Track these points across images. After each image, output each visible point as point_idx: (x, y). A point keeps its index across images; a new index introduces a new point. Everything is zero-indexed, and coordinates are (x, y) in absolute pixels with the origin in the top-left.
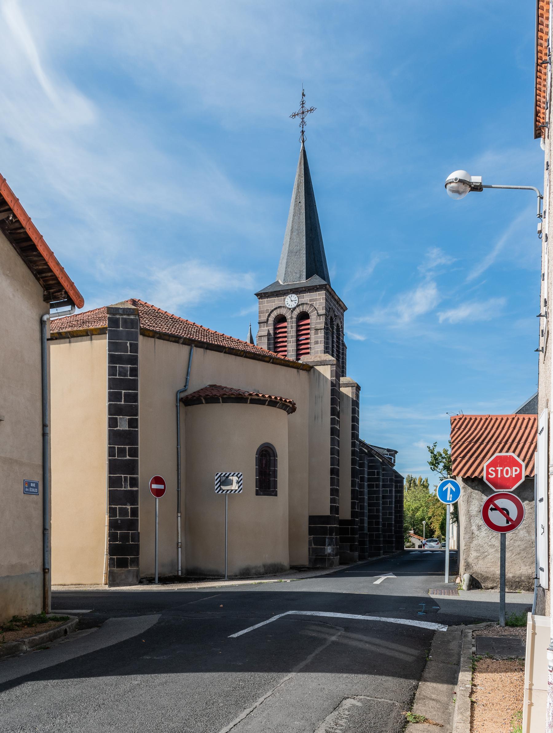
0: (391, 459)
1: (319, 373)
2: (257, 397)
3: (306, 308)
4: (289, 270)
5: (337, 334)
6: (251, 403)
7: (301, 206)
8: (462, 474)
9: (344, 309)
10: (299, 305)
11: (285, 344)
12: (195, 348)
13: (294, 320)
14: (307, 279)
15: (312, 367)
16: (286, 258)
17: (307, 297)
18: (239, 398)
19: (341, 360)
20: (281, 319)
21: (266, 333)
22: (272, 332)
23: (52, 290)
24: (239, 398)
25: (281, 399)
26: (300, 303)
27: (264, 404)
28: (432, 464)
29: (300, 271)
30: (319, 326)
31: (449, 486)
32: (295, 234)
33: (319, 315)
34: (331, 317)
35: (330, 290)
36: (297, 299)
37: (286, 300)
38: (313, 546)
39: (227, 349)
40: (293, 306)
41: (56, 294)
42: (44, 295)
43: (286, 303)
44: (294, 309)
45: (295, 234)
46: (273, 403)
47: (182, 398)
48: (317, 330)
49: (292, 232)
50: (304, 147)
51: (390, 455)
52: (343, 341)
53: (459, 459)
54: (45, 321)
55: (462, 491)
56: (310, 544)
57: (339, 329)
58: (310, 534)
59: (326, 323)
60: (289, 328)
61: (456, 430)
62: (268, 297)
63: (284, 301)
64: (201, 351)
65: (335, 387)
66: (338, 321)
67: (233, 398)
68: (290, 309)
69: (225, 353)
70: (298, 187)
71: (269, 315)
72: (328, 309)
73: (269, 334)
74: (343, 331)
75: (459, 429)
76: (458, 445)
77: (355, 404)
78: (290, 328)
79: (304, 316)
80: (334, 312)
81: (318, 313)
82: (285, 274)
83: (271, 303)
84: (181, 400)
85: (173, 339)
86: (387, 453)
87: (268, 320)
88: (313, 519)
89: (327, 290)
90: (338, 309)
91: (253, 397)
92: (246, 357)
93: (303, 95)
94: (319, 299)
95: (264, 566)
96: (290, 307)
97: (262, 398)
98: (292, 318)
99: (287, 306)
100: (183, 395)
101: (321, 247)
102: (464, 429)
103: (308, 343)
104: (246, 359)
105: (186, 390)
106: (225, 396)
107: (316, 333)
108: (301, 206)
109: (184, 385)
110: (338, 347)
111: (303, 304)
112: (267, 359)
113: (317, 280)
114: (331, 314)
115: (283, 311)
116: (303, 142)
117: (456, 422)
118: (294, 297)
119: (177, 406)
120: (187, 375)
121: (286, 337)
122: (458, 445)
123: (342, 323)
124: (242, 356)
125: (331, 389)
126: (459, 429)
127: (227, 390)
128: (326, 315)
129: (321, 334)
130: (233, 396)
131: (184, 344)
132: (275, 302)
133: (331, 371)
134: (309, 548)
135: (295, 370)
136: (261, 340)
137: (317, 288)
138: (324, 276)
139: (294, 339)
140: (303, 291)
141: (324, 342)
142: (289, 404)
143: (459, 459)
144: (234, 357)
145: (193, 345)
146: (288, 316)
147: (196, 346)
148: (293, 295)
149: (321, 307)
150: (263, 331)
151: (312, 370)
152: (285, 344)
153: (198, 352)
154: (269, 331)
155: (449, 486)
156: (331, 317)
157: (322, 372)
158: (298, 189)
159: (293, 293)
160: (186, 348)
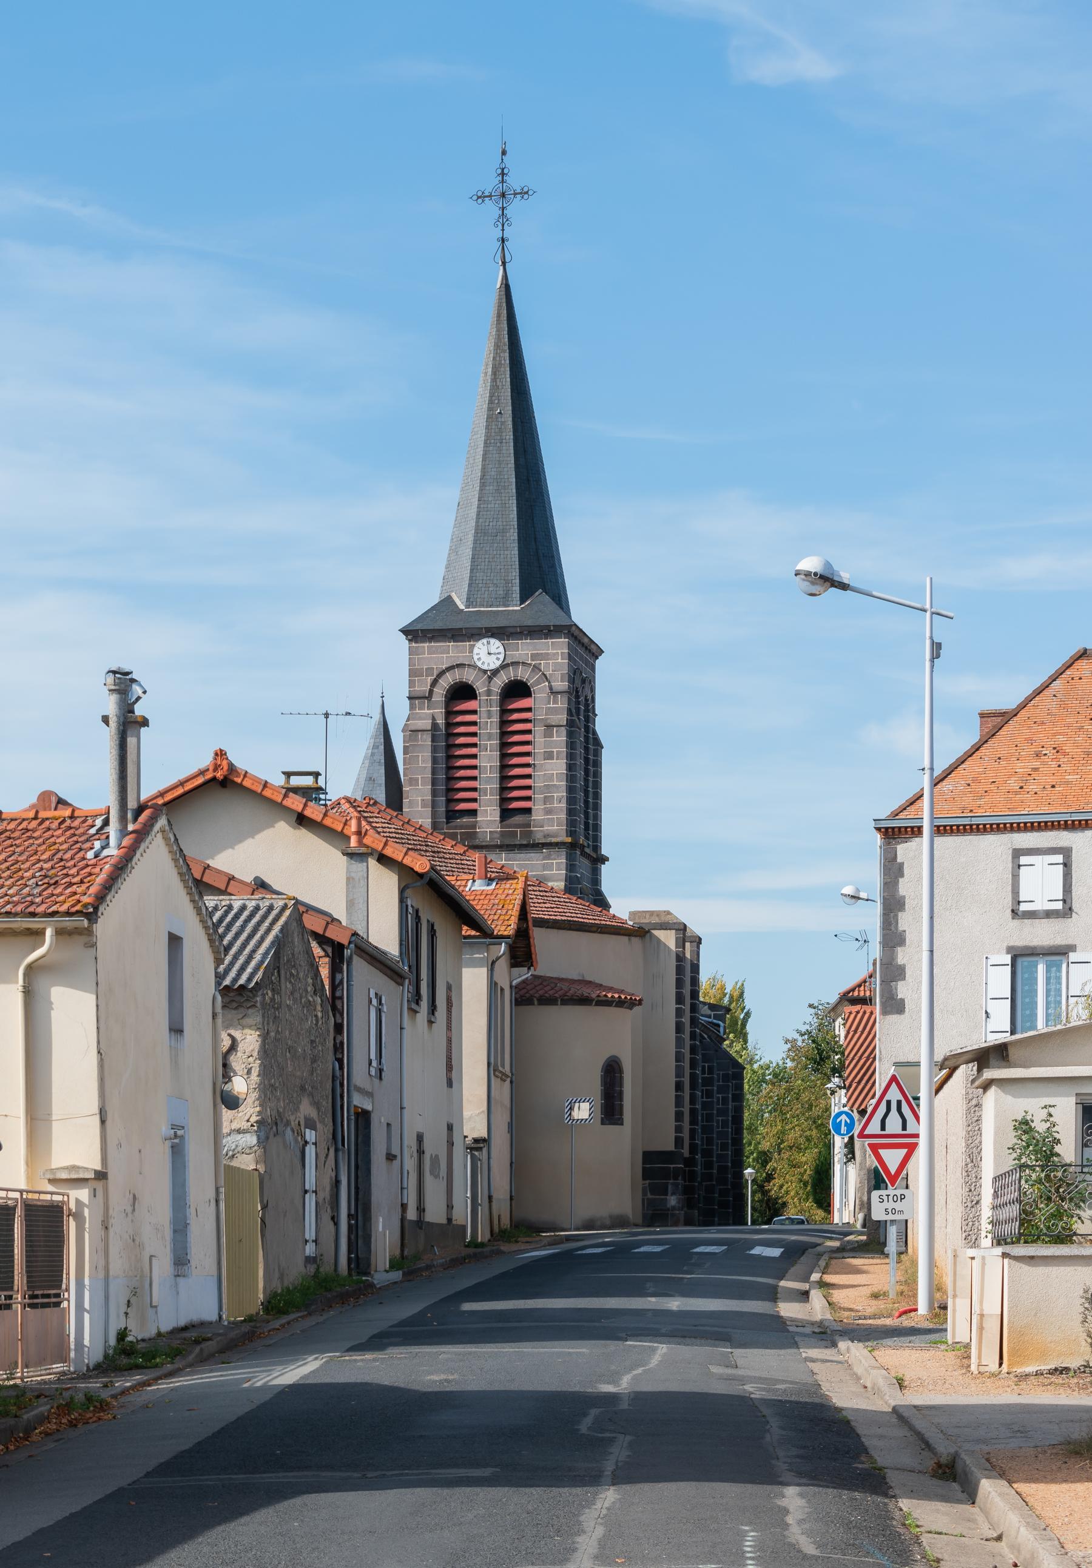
0: (719, 1026)
1: (659, 940)
4: (479, 575)
6: (596, 1005)
7: (503, 423)
8: (856, 1105)
10: (508, 665)
11: (473, 751)
13: (495, 698)
14: (522, 601)
15: (649, 932)
17: (525, 649)
20: (463, 692)
21: (427, 724)
22: (441, 721)
26: (508, 661)
28: (939, 1465)
29: (507, 582)
31: (844, 1117)
33: (553, 692)
35: (576, 633)
36: (501, 649)
37: (476, 650)
38: (649, 1196)
40: (493, 667)
43: (476, 657)
44: (495, 672)
45: (490, 488)
46: (620, 1003)
48: (549, 727)
49: (483, 485)
50: (505, 277)
51: (716, 1017)
52: (594, 733)
53: (854, 1085)
55: (857, 1123)
56: (644, 1193)
58: (644, 1178)
60: (484, 715)
61: (851, 1033)
63: (471, 651)
68: (485, 672)
70: (494, 373)
71: (434, 683)
73: (435, 726)
75: (855, 1031)
76: (854, 1062)
78: (486, 715)
79: (517, 690)
81: (551, 688)
82: (470, 585)
83: (442, 654)
86: (709, 1012)
87: (431, 692)
88: (649, 1157)
92: (570, 929)
94: (554, 653)
95: (611, 1217)
96: (485, 667)
98: (489, 692)
99: (479, 664)
102: (862, 1032)
108: (503, 423)
111: (515, 664)
112: (594, 929)
115: (469, 676)
116: (504, 263)
117: (852, 1016)
118: (495, 645)
121: (474, 734)
122: (854, 1062)
126: (855, 1031)
129: (560, 738)
133: (677, 939)
134: (643, 1200)
135: (626, 938)
136: (417, 740)
138: (560, 599)
139: (496, 742)
143: (854, 1085)
144: (555, 931)
146: (480, 687)
148: (492, 641)
149: (558, 674)
150: (420, 719)
152: (473, 751)
154: (434, 719)
155: (844, 1117)
157: (662, 939)
159: (493, 636)
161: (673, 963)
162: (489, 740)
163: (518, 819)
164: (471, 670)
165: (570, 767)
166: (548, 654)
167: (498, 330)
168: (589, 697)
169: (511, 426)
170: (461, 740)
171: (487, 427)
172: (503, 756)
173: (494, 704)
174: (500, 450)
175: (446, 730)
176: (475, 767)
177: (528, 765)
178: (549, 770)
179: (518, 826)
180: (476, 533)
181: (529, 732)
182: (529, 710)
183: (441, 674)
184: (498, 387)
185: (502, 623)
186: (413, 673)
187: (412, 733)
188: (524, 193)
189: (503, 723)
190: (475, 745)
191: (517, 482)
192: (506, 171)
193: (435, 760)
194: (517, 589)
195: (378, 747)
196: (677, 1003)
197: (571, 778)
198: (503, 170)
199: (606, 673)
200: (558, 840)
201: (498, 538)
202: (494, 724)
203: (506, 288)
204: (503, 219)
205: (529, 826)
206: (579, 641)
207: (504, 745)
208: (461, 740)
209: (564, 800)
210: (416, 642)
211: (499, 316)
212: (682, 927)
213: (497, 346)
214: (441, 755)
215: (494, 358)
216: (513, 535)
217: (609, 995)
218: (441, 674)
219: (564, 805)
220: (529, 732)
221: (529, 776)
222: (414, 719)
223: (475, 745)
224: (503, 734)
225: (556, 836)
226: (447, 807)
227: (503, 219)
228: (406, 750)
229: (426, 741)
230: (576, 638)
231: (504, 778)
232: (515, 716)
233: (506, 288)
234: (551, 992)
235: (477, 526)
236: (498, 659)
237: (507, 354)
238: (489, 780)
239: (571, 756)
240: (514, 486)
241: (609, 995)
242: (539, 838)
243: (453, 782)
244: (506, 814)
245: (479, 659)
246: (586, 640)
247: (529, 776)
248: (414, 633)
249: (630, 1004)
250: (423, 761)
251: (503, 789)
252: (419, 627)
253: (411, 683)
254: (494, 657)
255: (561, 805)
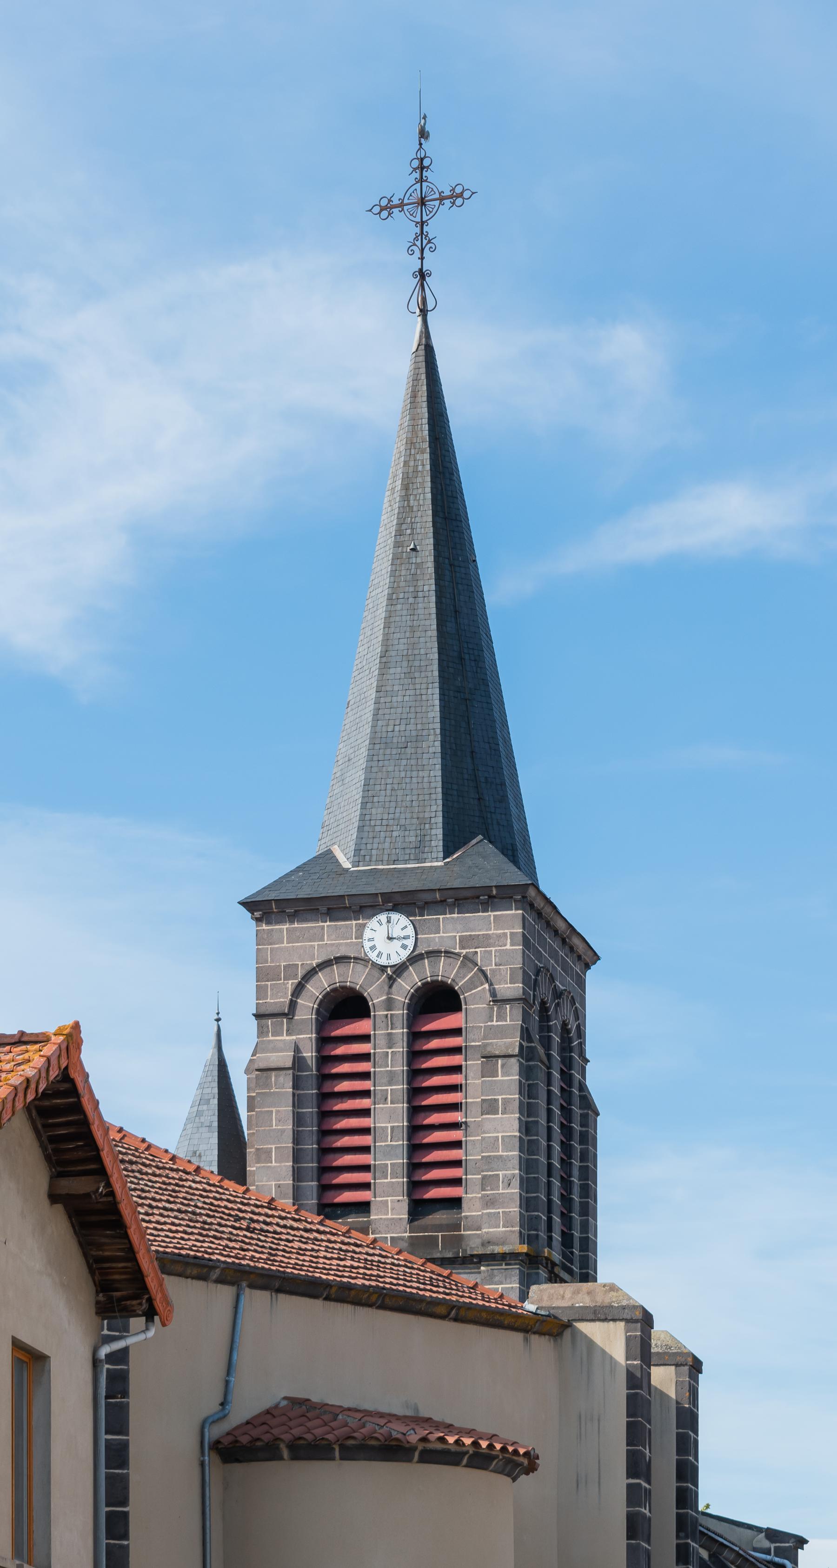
2: (439, 1446)
3: (445, 971)
4: (376, 812)
5: (563, 1061)
6: (422, 1460)
7: (418, 566)
9: (587, 958)
10: (420, 957)
11: (364, 1103)
12: (247, 1290)
13: (400, 1012)
14: (447, 853)
15: (568, 1325)
16: (362, 762)
17: (449, 929)
18: (384, 1444)
19: (576, 1163)
20: (347, 1005)
21: (285, 1058)
22: (309, 1054)
23: (118, 1294)
24: (384, 1444)
25: (504, 1449)
27: (457, 1463)
29: (422, 822)
30: (499, 1045)
32: (396, 671)
33: (497, 1000)
34: (543, 1003)
35: (539, 903)
36: (410, 931)
37: (368, 933)
39: (334, 1290)
40: (395, 960)
41: (128, 1302)
42: (98, 1303)
43: (367, 945)
44: (400, 969)
45: (396, 671)
46: (480, 1459)
47: (218, 1442)
48: (490, 1057)
49: (385, 666)
50: (426, 333)
51: (779, 1552)
52: (582, 1087)
54: (101, 1361)
57: (570, 1040)
59: (526, 1034)
60: (381, 1042)
62: (293, 917)
63: (360, 936)
64: (262, 1296)
65: (637, 1382)
66: (566, 1012)
67: (373, 1448)
68: (383, 968)
69: (327, 1299)
70: (406, 487)
71: (299, 989)
72: (534, 976)
73: (298, 1062)
74: (582, 1045)
77: (688, 1419)
78: (385, 1042)
79: (438, 999)
80: (552, 979)
81: (493, 993)
82: (360, 829)
83: (311, 942)
84: (216, 1446)
85: (195, 1272)
86: (766, 1544)
87: (293, 1005)
89: (529, 905)
90: (565, 967)
91: (430, 1446)
92: (383, 1307)
93: (423, 134)
94: (499, 937)
96: (383, 961)
97: (454, 1449)
98: (389, 1004)
99: (373, 956)
100: (216, 1432)
101: (498, 725)
103: (455, 1107)
104: (382, 1313)
105: (225, 1416)
106: (351, 1442)
107: (488, 1071)
109: (220, 1399)
110: (566, 1111)
111: (433, 954)
112: (442, 1310)
113: (483, 864)
114: (545, 992)
115: (355, 977)
116: (424, 312)
118: (400, 923)
119: (202, 1464)
120: (229, 1372)
121: (366, 1076)
123: (579, 1015)
124: (370, 1306)
125: (629, 1397)
127: (353, 1423)
128: (524, 1000)
129: (508, 1076)
130: (373, 1443)
131: (220, 1281)
132: (323, 938)
133: (628, 1340)
135: (518, 1337)
136: (267, 1085)
137: (491, 897)
138: (515, 847)
140: (436, 902)
141: (521, 1102)
142: (521, 1459)
144: (349, 1308)
145: (244, 1284)
146: (375, 996)
147: (252, 1286)
148: (395, 916)
149: (506, 970)
150: (275, 1050)
151: (567, 1333)
152: (364, 1103)
153: (256, 1301)
154: (297, 1050)
156: (543, 1003)
157: (598, 1340)
158: (406, 497)
159: (395, 908)
160: (226, 1293)
161: (620, 1391)
162: (390, 1083)
163: (440, 1217)
164: (359, 967)
165: (527, 1128)
166: (487, 937)
167: (413, 419)
168: (573, 1026)
169: (431, 570)
170: (345, 1086)
171: (393, 574)
172: (414, 1111)
173: (399, 1023)
174: (413, 609)
175: (318, 1069)
176: (366, 1131)
177: (455, 1126)
178: (492, 1131)
179: (439, 1228)
180: (373, 743)
181: (457, 1069)
182: (457, 1032)
183: (311, 973)
184: (411, 508)
185: (412, 884)
186: (263, 975)
187: (261, 1073)
188: (456, 196)
189: (414, 1055)
190: (366, 1094)
191: (440, 660)
192: (426, 163)
193: (298, 1120)
194: (439, 832)
195: (208, 1102)
196: (630, 1475)
197: (527, 1146)
198: (422, 160)
199: (605, 1001)
200: (506, 1249)
201: (408, 750)
202: (399, 1058)
203: (428, 354)
204: (423, 241)
205: (457, 1227)
206: (548, 923)
207: (415, 1092)
208: (345, 1086)
209: (516, 1182)
210: (269, 923)
211: (414, 395)
212: (638, 1315)
213: (411, 443)
214: (310, 1110)
215: (406, 463)
216: (434, 745)
217: (451, 1440)
218: (311, 973)
219: (515, 1190)
220: (457, 1069)
221: (457, 1144)
222: (264, 1051)
223: (366, 1094)
224: (414, 1073)
225: (503, 1244)
226: (320, 1197)
227: (423, 241)
228: (251, 1104)
229: (284, 1085)
230: (539, 914)
231: (415, 1148)
232: (435, 1043)
233: (428, 354)
234: (318, 1432)
235: (374, 732)
236: (404, 947)
237: (427, 456)
238: (390, 1151)
239: (527, 1109)
240: (435, 667)
241: (451, 1440)
242: (474, 1247)
243: (330, 1156)
244: (419, 1208)
245: (373, 948)
246: (561, 925)
247: (457, 1144)
248: (263, 908)
249: (516, 1464)
250: (279, 1121)
251: (414, 1167)
252: (272, 896)
253: (261, 992)
254: (397, 944)
255: (510, 1192)
